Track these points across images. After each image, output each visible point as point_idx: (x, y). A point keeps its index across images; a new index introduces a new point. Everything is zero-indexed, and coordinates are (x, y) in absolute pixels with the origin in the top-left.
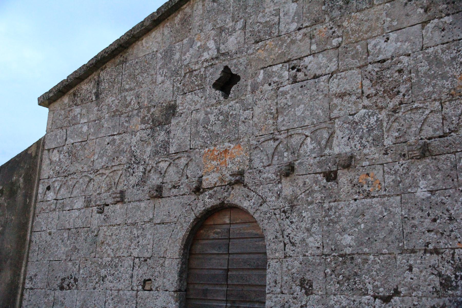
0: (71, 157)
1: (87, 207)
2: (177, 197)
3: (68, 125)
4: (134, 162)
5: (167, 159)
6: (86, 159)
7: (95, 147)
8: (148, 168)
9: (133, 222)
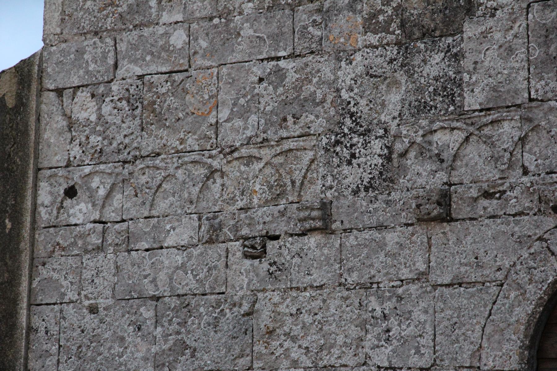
0: (138, 112)
1: (210, 241)
2: (499, 221)
3: (120, 25)
4: (350, 129)
5: (458, 124)
6: (190, 119)
7: (218, 89)
8: (399, 147)
9: (365, 279)
